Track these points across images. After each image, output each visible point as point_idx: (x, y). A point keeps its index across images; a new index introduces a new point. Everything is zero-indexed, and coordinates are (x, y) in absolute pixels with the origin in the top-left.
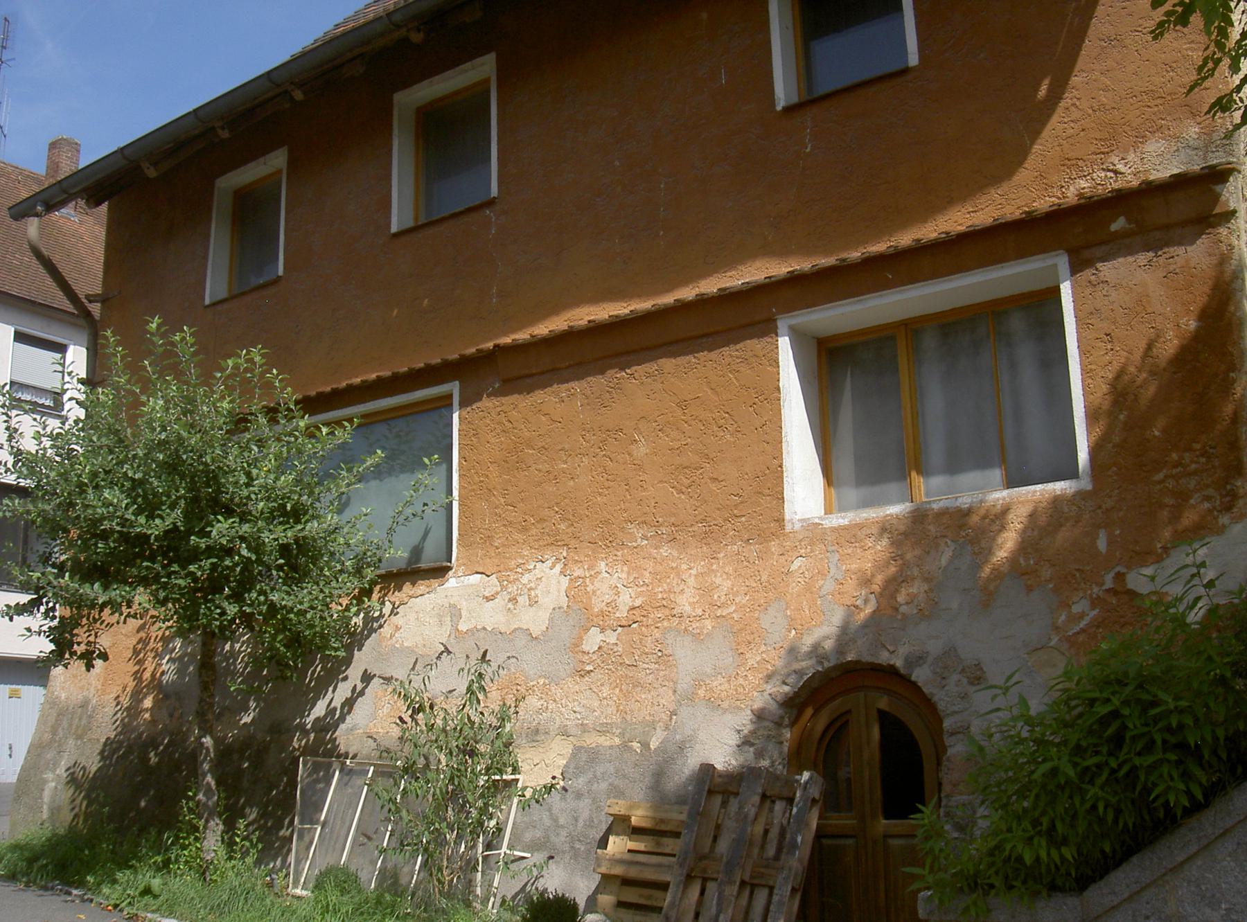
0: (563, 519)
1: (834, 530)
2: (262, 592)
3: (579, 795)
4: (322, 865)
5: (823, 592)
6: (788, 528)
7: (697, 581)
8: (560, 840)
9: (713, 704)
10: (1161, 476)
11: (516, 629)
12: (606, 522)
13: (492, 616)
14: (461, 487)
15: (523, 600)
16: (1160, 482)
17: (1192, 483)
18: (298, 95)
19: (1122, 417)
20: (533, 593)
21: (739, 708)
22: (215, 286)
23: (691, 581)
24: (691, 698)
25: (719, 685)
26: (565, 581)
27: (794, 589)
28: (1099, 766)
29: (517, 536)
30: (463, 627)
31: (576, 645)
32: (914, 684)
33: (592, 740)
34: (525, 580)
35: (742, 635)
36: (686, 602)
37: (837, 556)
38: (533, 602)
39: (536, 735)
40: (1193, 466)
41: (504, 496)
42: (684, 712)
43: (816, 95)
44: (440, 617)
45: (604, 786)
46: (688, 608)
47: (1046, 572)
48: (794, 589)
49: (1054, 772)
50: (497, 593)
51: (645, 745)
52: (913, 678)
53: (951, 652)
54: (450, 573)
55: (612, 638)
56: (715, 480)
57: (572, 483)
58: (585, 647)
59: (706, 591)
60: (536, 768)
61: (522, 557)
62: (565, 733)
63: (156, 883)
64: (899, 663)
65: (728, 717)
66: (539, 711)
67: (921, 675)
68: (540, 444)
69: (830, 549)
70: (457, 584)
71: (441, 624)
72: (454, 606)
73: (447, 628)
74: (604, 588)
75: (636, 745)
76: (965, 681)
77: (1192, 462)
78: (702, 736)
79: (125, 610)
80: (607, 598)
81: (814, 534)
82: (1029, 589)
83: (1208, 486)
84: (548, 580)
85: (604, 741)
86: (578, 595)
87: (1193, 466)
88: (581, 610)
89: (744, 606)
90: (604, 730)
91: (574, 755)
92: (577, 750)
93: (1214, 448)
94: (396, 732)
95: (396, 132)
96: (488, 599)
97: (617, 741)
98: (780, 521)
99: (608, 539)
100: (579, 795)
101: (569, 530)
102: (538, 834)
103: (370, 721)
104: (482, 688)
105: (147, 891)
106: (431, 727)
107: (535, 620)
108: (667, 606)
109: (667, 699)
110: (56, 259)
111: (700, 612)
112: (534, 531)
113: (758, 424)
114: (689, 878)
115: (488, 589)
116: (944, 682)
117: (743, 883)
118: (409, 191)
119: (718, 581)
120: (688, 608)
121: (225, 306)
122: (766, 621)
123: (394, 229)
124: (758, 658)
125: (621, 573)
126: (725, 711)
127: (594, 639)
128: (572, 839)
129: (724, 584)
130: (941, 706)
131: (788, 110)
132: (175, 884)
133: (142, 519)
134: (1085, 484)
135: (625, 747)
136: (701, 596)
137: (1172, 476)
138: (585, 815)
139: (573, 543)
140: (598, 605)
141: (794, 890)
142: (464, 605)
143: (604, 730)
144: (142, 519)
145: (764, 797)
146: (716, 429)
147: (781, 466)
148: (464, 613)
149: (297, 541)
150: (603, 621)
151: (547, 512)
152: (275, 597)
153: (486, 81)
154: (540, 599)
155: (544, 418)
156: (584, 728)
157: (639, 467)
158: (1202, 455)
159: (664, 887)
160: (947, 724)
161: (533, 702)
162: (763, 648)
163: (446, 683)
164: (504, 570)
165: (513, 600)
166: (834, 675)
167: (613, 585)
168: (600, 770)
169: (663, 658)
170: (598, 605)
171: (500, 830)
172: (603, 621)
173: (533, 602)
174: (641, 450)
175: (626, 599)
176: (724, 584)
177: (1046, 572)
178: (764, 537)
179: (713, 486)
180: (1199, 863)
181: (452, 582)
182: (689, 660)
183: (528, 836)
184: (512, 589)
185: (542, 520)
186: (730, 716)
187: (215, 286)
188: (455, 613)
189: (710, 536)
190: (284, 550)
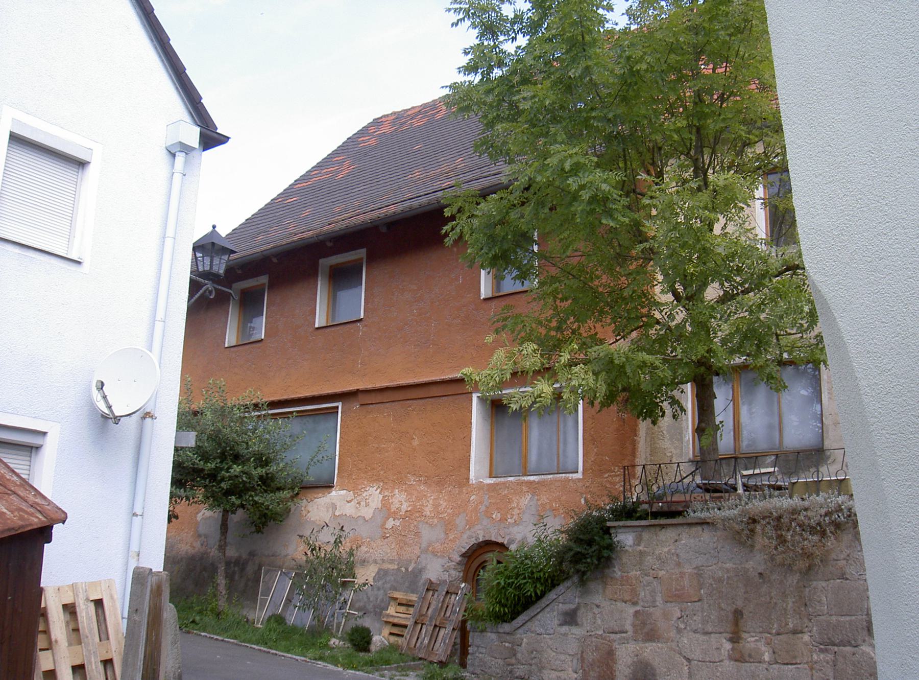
1: (488, 485)
2: (251, 496)
3: (379, 589)
4: (269, 613)
7: (433, 501)
8: (370, 607)
9: (434, 554)
13: (349, 510)
15: (363, 503)
18: (275, 260)
22: (231, 338)
23: (431, 502)
24: (426, 551)
25: (438, 546)
26: (381, 497)
27: (470, 508)
28: (513, 583)
30: (337, 514)
31: (383, 526)
33: (386, 566)
35: (449, 526)
36: (428, 511)
38: (367, 505)
39: (364, 562)
42: (423, 556)
43: (501, 294)
44: (328, 508)
45: (389, 585)
46: (428, 513)
48: (470, 508)
49: (499, 583)
51: (407, 569)
55: (398, 523)
58: (387, 526)
59: (436, 506)
60: (365, 575)
62: (375, 562)
63: (198, 618)
65: (439, 560)
66: (366, 552)
70: (335, 494)
73: (331, 513)
74: (396, 501)
75: (403, 569)
78: (429, 567)
79: (192, 501)
80: (397, 506)
81: (480, 486)
82: (555, 516)
84: (374, 495)
85: (391, 567)
86: (386, 503)
88: (386, 510)
90: (392, 562)
91: (378, 573)
92: (380, 570)
94: (304, 558)
95: (319, 278)
96: (348, 502)
97: (396, 567)
99: (400, 481)
100: (379, 589)
102: (362, 604)
103: (295, 550)
104: (340, 542)
105: (193, 622)
106: (318, 557)
107: (367, 513)
108: (421, 512)
109: (417, 551)
114: (416, 623)
117: (435, 626)
118: (325, 307)
120: (428, 513)
121: (235, 349)
122: (457, 522)
123: (317, 326)
125: (403, 496)
127: (390, 523)
128: (374, 607)
129: (444, 504)
131: (485, 299)
132: (206, 619)
133: (202, 463)
135: (399, 569)
138: (380, 597)
139: (386, 481)
140: (393, 509)
141: (454, 629)
143: (392, 562)
144: (202, 463)
145: (447, 592)
149: (267, 474)
150: (394, 515)
152: (256, 499)
153: (362, 259)
156: (383, 561)
159: (405, 626)
161: (364, 548)
163: (326, 538)
164: (355, 488)
165: (359, 503)
167: (400, 500)
168: (388, 579)
169: (417, 534)
170: (393, 509)
171: (345, 602)
172: (394, 515)
175: (405, 507)
176: (444, 504)
181: (334, 493)
182: (428, 534)
183: (357, 605)
187: (231, 338)
188: (334, 507)
189: (440, 483)
190: (261, 478)
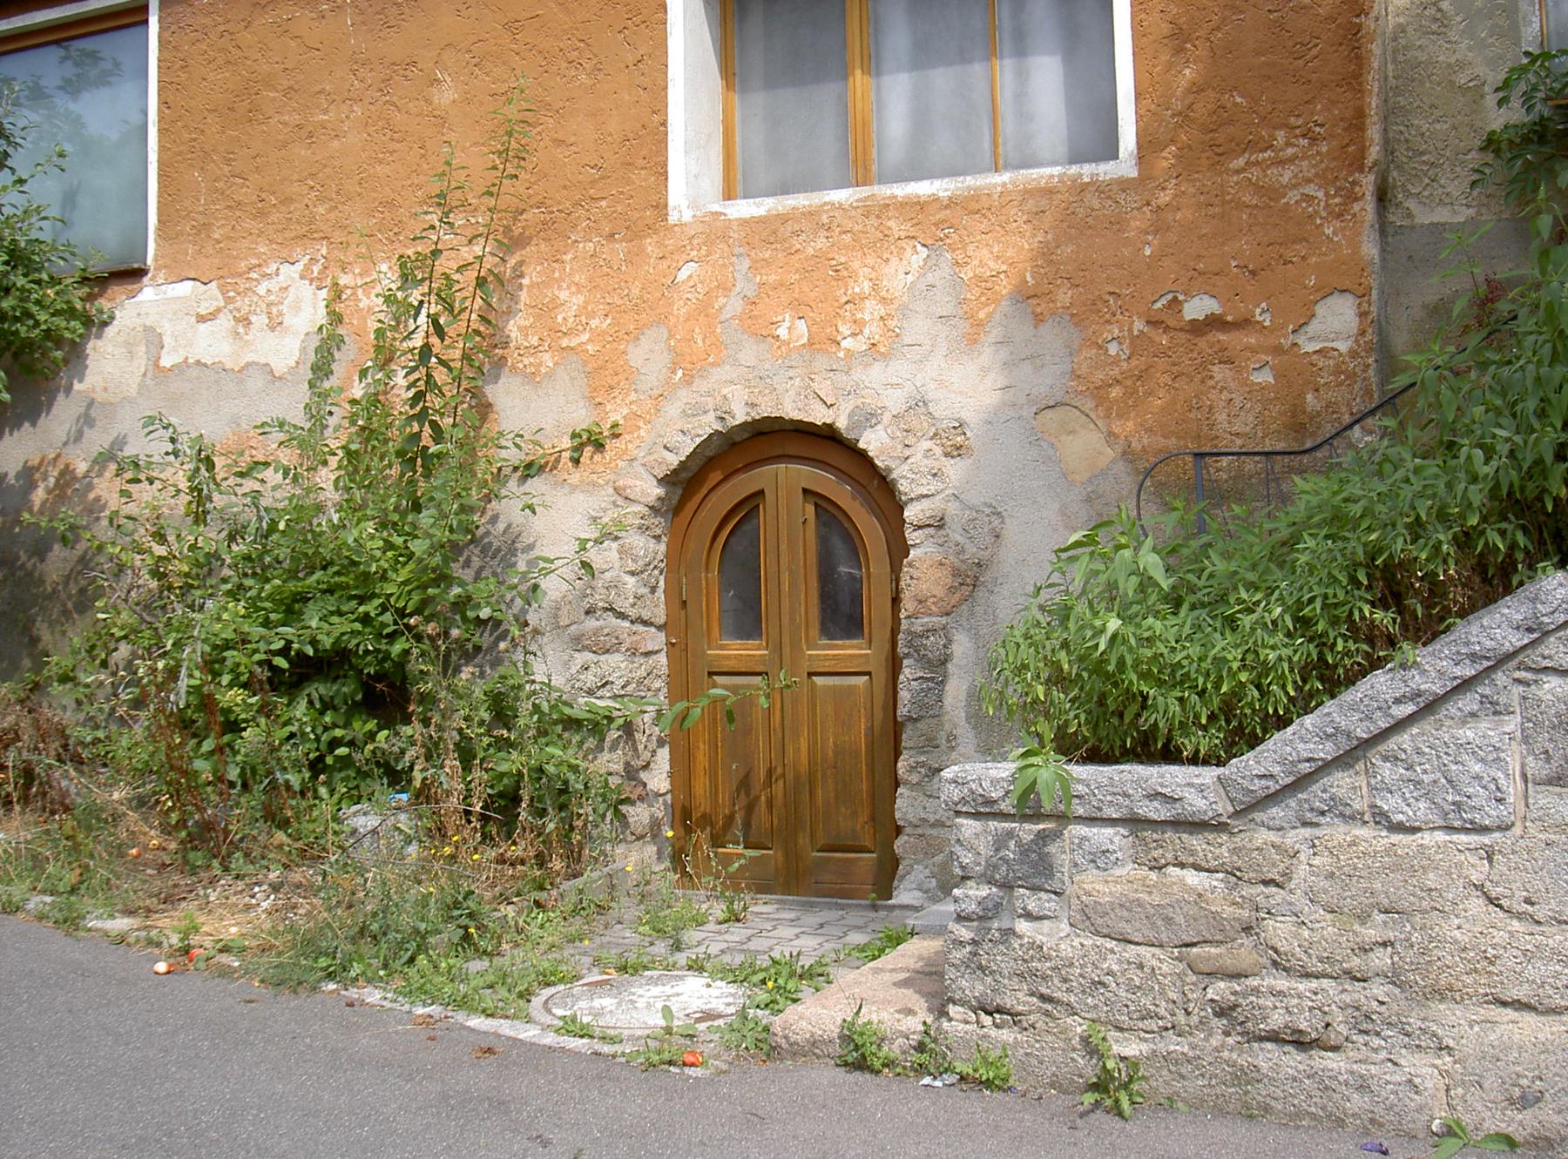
0: (321, 200)
1: (744, 222)
5: (725, 315)
6: (673, 218)
10: (1241, 162)
11: (248, 365)
12: (390, 204)
14: (162, 149)
15: (259, 321)
16: (1237, 172)
17: (1287, 176)
19: (1187, 72)
20: (274, 310)
21: (594, 484)
27: (680, 310)
29: (248, 224)
30: (166, 362)
32: (863, 456)
34: (261, 290)
37: (747, 263)
38: (275, 325)
40: (1290, 151)
41: (228, 162)
47: (1064, 296)
50: (219, 310)
52: (861, 445)
53: (920, 403)
54: (146, 280)
56: (559, 142)
57: (336, 143)
61: (258, 256)
64: (842, 424)
67: (872, 442)
68: (286, 84)
69: (737, 250)
71: (131, 354)
72: (149, 330)
76: (938, 451)
77: (1288, 144)
81: (714, 232)
82: (1038, 319)
83: (1309, 181)
87: (1290, 151)
89: (604, 332)
93: (1322, 126)
96: (202, 319)
98: (661, 207)
101: (332, 216)
110: (1135, 492)
111: (535, 341)
112: (274, 217)
113: (630, 59)
115: (204, 304)
116: (907, 452)
119: (564, 295)
124: (625, 411)
126: (574, 488)
130: (903, 486)
134: (1125, 165)
136: (538, 317)
137: (1257, 163)
139: (338, 236)
142: (166, 328)
146: (565, 65)
147: (664, 124)
148: (167, 340)
151: (296, 188)
154: (287, 320)
155: (293, 44)
157: (442, 121)
158: (1304, 136)
160: (908, 513)
162: (633, 397)
164: (228, 274)
165: (246, 321)
166: (738, 438)
173: (275, 325)
174: (446, 95)
177: (1064, 296)
178: (635, 233)
179: (559, 152)
180: (1415, 731)
184: (243, 304)
185: (288, 200)
186: (581, 497)
